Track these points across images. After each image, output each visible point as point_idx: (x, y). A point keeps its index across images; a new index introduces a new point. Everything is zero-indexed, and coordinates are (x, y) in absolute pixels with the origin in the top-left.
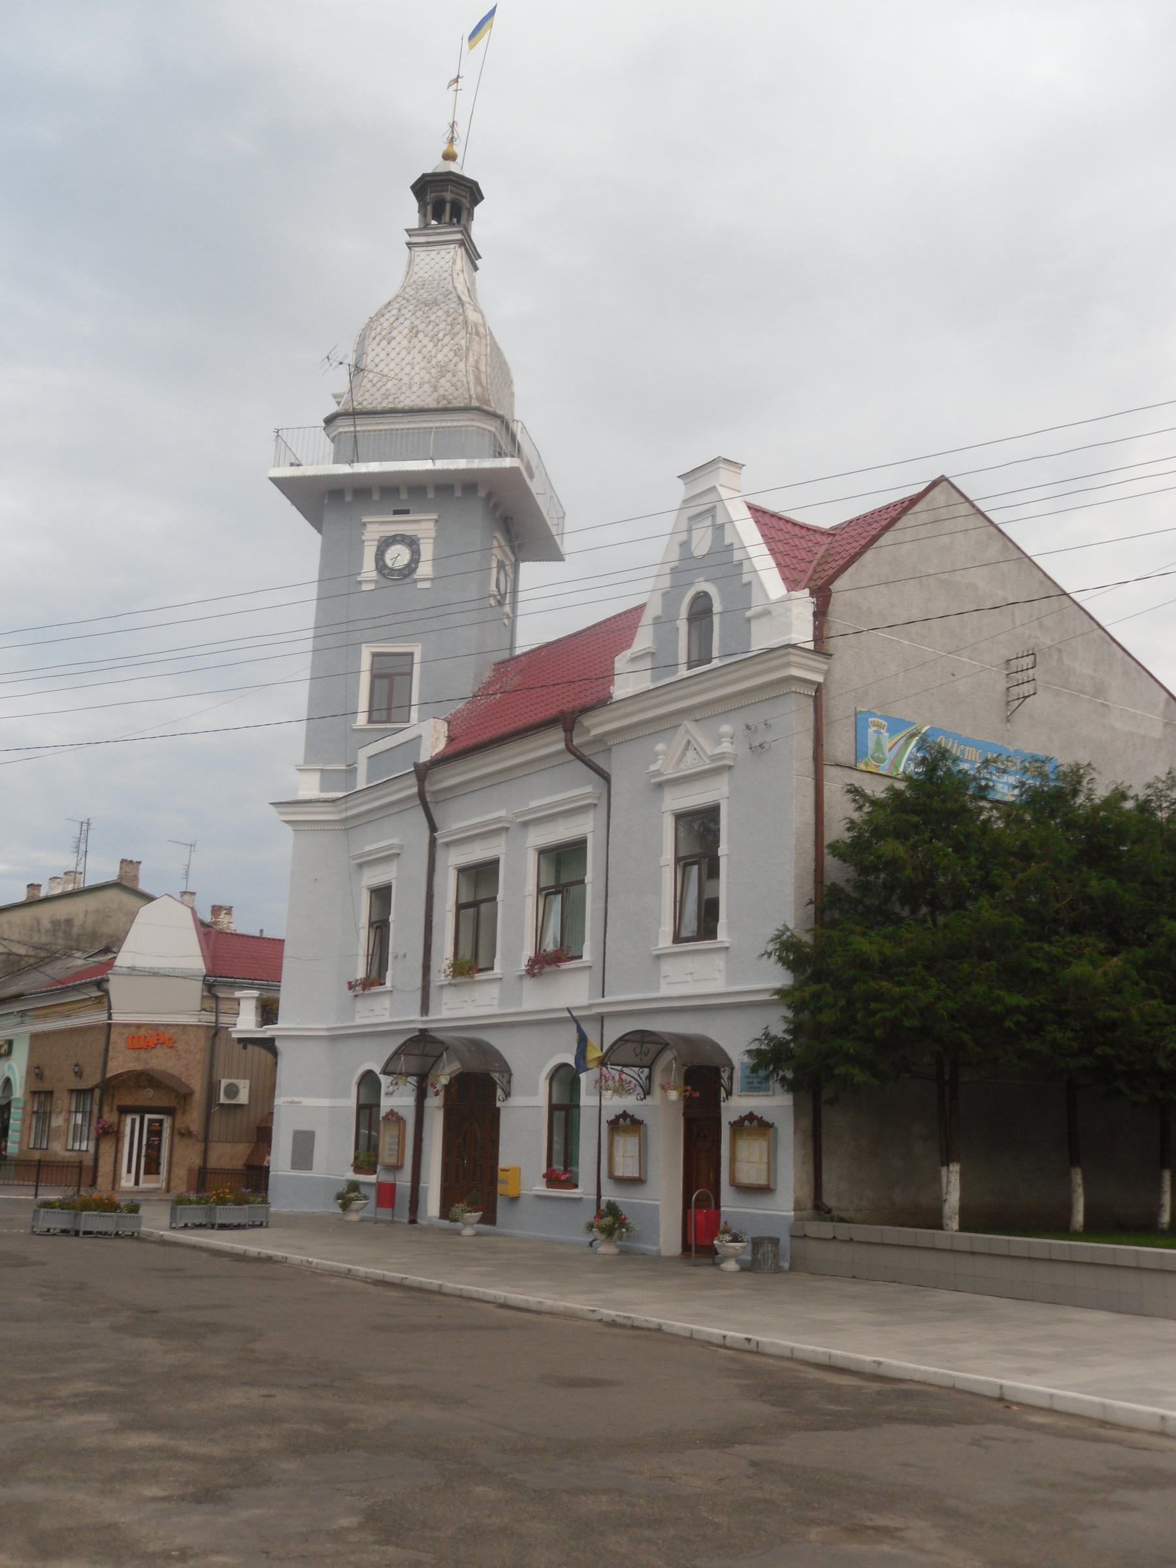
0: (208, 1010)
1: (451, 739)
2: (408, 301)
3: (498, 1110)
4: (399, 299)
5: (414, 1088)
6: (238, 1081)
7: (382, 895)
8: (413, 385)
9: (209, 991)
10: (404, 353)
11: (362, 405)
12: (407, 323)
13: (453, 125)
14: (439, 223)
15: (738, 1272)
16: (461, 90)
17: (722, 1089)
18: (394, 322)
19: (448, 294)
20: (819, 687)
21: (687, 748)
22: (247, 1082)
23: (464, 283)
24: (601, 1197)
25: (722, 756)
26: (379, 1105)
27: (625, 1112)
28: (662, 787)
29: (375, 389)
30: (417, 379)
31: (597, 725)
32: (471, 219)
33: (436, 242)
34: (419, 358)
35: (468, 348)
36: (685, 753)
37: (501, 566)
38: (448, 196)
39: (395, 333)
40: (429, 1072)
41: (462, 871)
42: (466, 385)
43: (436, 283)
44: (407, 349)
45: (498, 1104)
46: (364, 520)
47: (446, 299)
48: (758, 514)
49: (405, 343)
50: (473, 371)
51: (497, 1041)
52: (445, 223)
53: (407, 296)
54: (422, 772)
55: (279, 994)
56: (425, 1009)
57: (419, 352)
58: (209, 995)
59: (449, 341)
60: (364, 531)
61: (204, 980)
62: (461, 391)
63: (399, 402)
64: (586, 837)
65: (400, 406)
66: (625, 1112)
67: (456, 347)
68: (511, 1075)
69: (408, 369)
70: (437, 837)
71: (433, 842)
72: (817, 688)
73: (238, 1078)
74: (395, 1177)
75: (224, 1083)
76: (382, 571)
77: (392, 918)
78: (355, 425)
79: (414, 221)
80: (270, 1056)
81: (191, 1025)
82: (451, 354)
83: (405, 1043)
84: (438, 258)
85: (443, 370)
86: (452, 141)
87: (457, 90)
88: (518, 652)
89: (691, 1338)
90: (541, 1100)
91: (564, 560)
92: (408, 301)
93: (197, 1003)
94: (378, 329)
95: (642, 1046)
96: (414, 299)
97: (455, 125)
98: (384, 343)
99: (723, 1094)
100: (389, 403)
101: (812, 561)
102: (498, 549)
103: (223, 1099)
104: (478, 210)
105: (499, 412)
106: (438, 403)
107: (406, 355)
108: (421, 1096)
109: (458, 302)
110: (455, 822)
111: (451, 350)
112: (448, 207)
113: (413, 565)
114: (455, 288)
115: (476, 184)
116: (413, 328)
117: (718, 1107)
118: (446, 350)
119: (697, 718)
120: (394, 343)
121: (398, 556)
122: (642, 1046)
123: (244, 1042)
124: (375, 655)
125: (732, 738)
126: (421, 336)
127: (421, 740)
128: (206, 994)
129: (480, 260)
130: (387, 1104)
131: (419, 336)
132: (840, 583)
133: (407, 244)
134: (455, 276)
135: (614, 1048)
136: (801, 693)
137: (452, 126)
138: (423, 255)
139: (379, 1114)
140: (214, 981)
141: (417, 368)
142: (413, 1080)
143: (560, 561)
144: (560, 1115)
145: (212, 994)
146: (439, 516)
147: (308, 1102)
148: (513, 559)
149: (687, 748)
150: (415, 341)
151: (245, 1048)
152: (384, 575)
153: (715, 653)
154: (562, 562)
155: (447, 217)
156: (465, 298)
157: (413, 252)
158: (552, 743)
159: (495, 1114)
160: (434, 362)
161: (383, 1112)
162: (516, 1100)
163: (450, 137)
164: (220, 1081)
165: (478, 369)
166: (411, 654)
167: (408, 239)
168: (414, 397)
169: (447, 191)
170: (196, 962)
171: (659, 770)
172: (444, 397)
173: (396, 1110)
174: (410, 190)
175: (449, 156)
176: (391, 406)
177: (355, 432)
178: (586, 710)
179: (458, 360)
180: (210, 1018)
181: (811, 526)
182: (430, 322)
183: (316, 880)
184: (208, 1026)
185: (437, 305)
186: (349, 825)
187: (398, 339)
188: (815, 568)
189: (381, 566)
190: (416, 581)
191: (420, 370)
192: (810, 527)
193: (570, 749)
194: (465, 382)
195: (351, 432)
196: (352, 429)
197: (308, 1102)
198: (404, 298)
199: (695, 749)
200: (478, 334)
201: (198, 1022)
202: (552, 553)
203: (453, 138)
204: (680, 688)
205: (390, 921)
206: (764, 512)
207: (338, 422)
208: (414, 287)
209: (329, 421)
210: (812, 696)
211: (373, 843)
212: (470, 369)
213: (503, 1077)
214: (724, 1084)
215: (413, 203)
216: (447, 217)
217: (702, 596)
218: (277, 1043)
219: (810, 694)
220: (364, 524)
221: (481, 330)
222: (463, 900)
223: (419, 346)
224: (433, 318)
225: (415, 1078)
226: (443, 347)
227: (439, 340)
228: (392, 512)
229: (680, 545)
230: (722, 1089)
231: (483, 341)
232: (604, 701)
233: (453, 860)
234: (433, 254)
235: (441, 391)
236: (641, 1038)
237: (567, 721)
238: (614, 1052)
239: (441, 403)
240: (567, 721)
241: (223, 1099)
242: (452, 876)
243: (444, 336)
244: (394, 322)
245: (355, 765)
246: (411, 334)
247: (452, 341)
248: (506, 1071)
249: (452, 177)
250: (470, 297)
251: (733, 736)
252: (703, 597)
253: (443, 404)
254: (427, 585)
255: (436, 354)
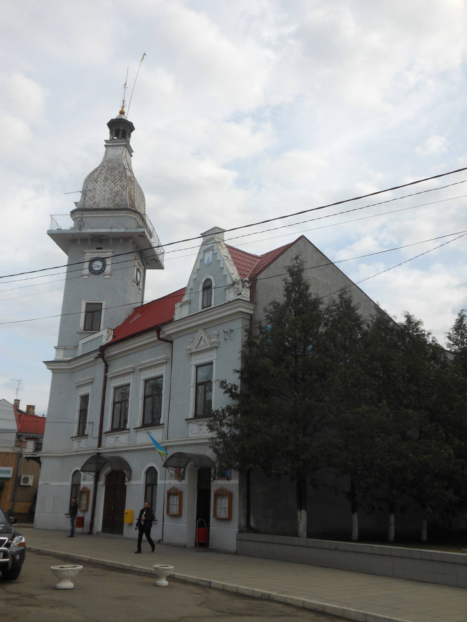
0: (18, 446)
1: (114, 337)
2: (104, 167)
3: (126, 486)
4: (101, 167)
5: (94, 477)
6: (29, 476)
7: (85, 399)
8: (105, 199)
9: (19, 439)
10: (102, 187)
11: (85, 207)
12: (104, 176)
13: (124, 101)
14: (118, 138)
15: (192, 548)
16: (127, 88)
17: (212, 477)
18: (98, 175)
19: (120, 165)
20: (251, 315)
21: (201, 340)
22: (33, 476)
23: (126, 161)
24: (164, 523)
25: (214, 343)
26: (80, 485)
27: (174, 487)
28: (192, 355)
29: (91, 201)
30: (107, 197)
31: (168, 330)
32: (130, 137)
33: (115, 145)
34: (108, 189)
35: (127, 186)
36: (200, 342)
37: (138, 270)
38: (121, 128)
39: (99, 179)
40: (100, 470)
41: (116, 389)
42: (126, 200)
43: (115, 161)
44: (103, 186)
45: (126, 484)
46: (85, 251)
47: (119, 167)
48: (231, 249)
49: (103, 183)
50: (129, 195)
51: (127, 457)
52: (120, 138)
53: (104, 165)
54: (103, 349)
55: (43, 439)
56: (100, 445)
57: (108, 187)
58: (19, 440)
59: (120, 183)
60: (84, 256)
61: (17, 434)
62: (123, 202)
63: (100, 206)
64: (163, 375)
65: (100, 207)
66: (174, 487)
67: (122, 185)
68: (131, 471)
69: (103, 193)
70: (107, 375)
71: (106, 378)
72: (251, 316)
73: (29, 475)
74: (84, 514)
75: (23, 477)
76: (91, 271)
77: (88, 408)
78: (82, 215)
79: (108, 137)
80: (37, 464)
81: (10, 453)
82: (121, 188)
83: (90, 459)
84: (116, 151)
85: (117, 194)
86: (123, 107)
87: (125, 88)
88: (144, 303)
89: (141, 572)
90: (142, 481)
91: (161, 267)
92: (104, 167)
93: (13, 444)
94: (92, 178)
95: (180, 459)
96: (107, 166)
97: (124, 101)
98: (95, 183)
99: (212, 479)
100: (95, 206)
101: (252, 268)
102: (137, 263)
103: (22, 484)
104: (133, 134)
105: (138, 211)
106: (115, 207)
107: (103, 188)
108: (97, 479)
109: (124, 168)
110: (114, 370)
111: (120, 186)
112: (121, 132)
113: (103, 269)
114: (123, 163)
115: (132, 123)
116: (106, 178)
117: (210, 484)
118: (118, 186)
119: (205, 328)
120: (98, 183)
121: (98, 265)
122: (180, 459)
123: (28, 459)
124: (87, 304)
125: (218, 336)
126: (109, 180)
127: (103, 337)
128: (17, 440)
129: (133, 153)
130: (83, 484)
131: (108, 181)
132: (261, 276)
133: (105, 146)
134: (123, 158)
135: (169, 460)
136: (243, 318)
137: (123, 102)
138: (111, 150)
139: (80, 488)
140: (21, 435)
141: (107, 193)
142: (93, 474)
143: (162, 269)
144: (149, 488)
145: (20, 440)
146: (114, 251)
147: (52, 483)
148: (143, 268)
149: (201, 340)
150: (107, 182)
151: (28, 461)
152: (92, 273)
153: (213, 303)
154: (163, 270)
155: (120, 136)
156: (126, 167)
157: (107, 149)
158: (152, 338)
159: (125, 488)
160: (113, 191)
161: (81, 487)
162: (133, 482)
163: (123, 105)
164: (21, 476)
165: (130, 194)
166: (102, 304)
167: (105, 144)
168: (105, 204)
169: (120, 126)
170: (14, 426)
171: (190, 348)
172: (117, 204)
173: (86, 486)
174: (107, 125)
175: (122, 113)
176: (96, 207)
177: (82, 217)
178: (164, 324)
179: (123, 190)
180: (17, 450)
181: (252, 254)
182: (112, 175)
183: (60, 392)
184: (17, 453)
185: (115, 169)
186: (72, 371)
187: (100, 182)
188: (253, 270)
189: (91, 269)
190: (104, 275)
191: (108, 194)
192: (252, 255)
193: (160, 339)
194: (125, 199)
195: (80, 217)
196: (81, 216)
197: (52, 483)
198: (103, 166)
199: (204, 340)
200: (131, 180)
201: (14, 451)
202: (159, 266)
203: (123, 105)
204: (198, 316)
205: (88, 409)
206: (234, 249)
207: (75, 213)
208: (107, 162)
209: (73, 213)
210: (249, 319)
211: (81, 377)
212: (127, 194)
213: (128, 472)
214: (212, 475)
215: (108, 130)
216: (120, 136)
217: (208, 280)
218: (41, 459)
219: (248, 318)
220: (85, 253)
221: (132, 179)
222: (117, 400)
223: (108, 184)
224: (113, 174)
225: (94, 473)
226: (117, 185)
227: (116, 183)
228: (96, 248)
229: (201, 261)
230: (212, 477)
231: (133, 183)
232: (171, 321)
233: (113, 384)
234: (115, 150)
235: (116, 202)
236: (180, 455)
237: (158, 329)
238: (169, 461)
239: (116, 207)
240: (158, 329)
241: (22, 484)
242: (112, 391)
243: (118, 181)
244: (98, 175)
245: (78, 347)
246: (105, 180)
247: (120, 183)
248: (130, 470)
249: (131, 125)
250: (129, 166)
251: (218, 335)
252: (208, 280)
253: (117, 207)
254: (108, 277)
255: (114, 188)
